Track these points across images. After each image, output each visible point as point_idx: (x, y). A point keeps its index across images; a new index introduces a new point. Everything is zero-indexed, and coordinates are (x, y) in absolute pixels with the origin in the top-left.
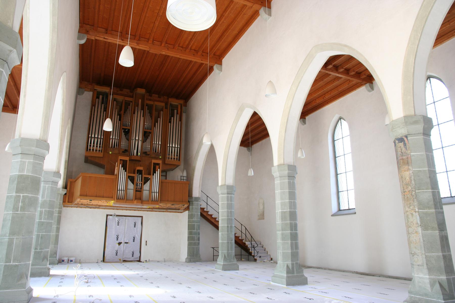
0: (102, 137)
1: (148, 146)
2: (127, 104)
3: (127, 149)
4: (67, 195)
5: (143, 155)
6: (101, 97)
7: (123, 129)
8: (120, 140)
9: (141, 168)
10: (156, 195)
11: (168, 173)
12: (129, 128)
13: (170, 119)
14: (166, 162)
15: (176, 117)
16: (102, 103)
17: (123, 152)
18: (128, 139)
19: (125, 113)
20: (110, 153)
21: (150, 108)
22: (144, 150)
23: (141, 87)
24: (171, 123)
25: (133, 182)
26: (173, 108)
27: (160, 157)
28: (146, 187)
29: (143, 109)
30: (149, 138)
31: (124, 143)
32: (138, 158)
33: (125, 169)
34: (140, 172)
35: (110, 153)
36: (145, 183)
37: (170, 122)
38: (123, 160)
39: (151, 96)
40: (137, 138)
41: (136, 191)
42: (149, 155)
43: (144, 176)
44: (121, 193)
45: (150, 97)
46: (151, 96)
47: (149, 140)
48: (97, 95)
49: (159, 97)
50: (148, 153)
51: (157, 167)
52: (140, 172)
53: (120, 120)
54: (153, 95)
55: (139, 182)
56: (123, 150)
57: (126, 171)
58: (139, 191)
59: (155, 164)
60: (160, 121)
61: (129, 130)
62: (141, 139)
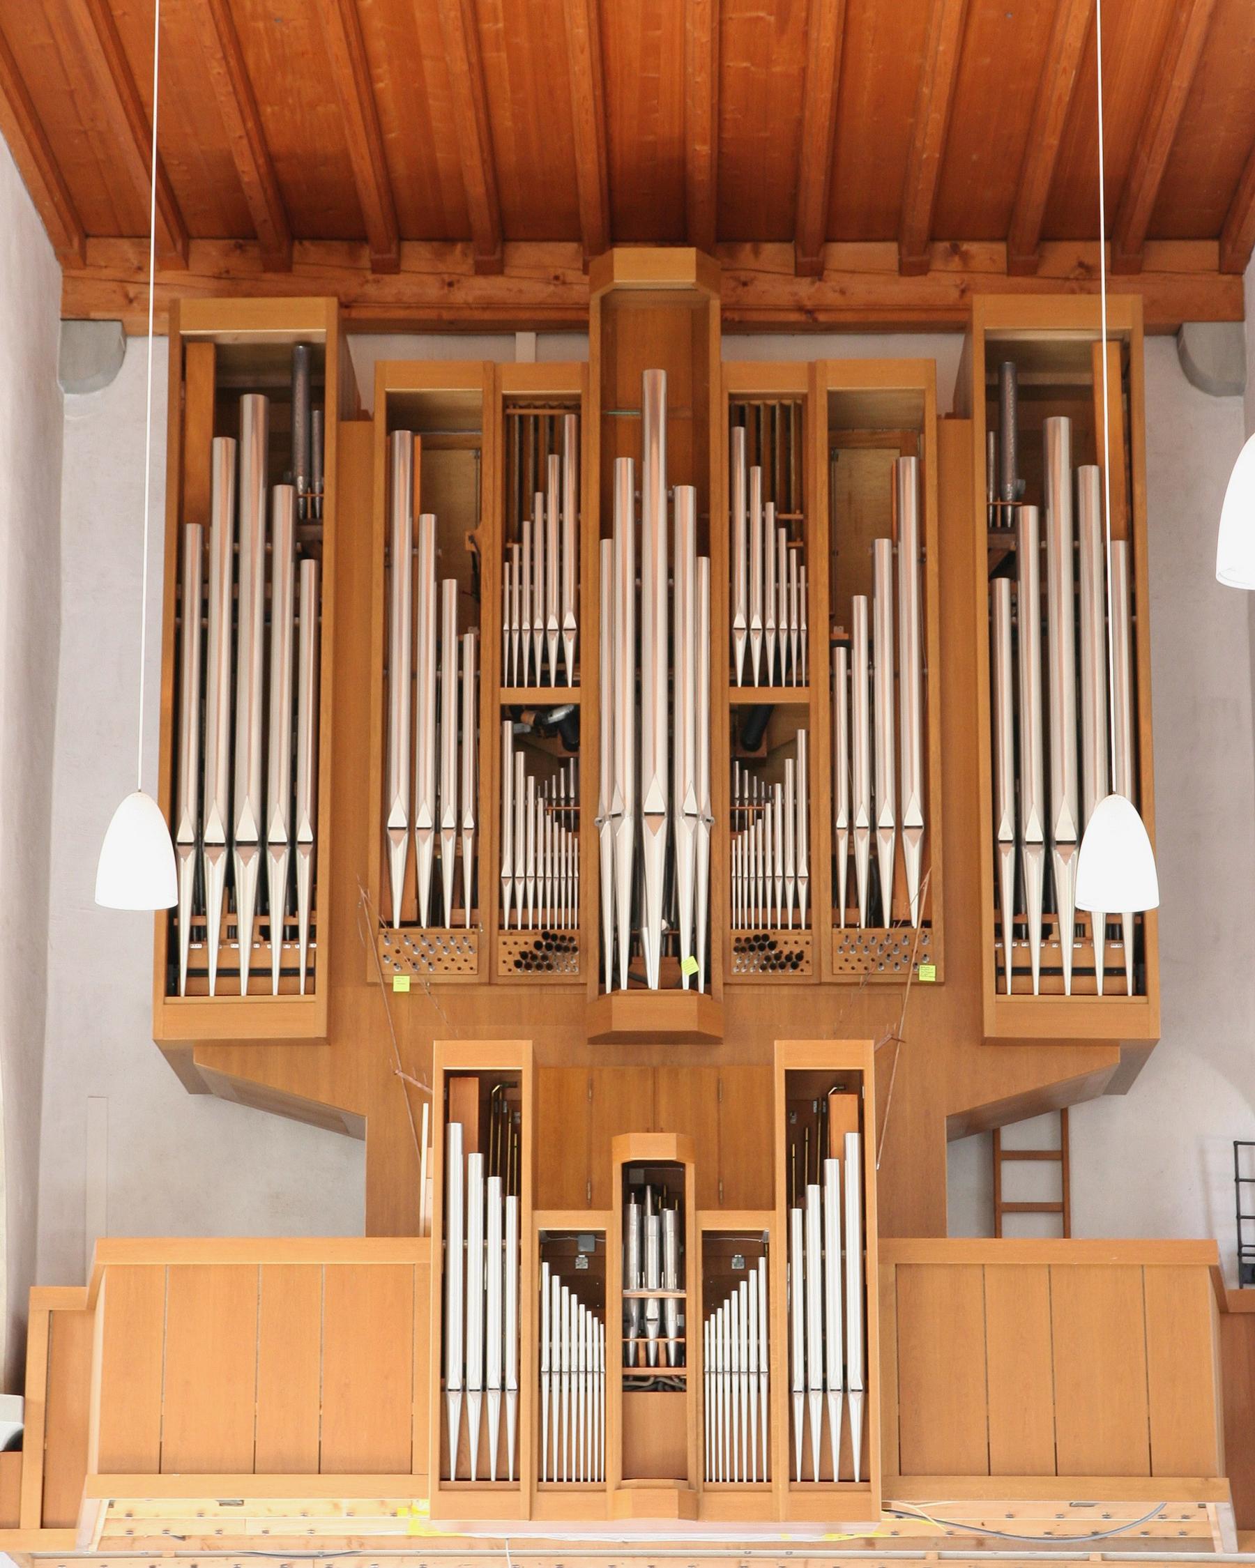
0: (305, 834)
1: (780, 853)
2: (530, 435)
3: (561, 917)
4: (32, 1444)
5: (745, 967)
6: (252, 408)
7: (512, 712)
8: (489, 830)
9: (658, 1147)
10: (837, 1417)
11: (1078, 1117)
12: (568, 695)
13: (1002, 525)
14: (989, 1032)
15: (1076, 492)
16: (277, 472)
17: (525, 961)
18: (570, 821)
19: (512, 534)
20: (401, 984)
21: (772, 429)
22: (749, 918)
23: (671, 234)
24: (1014, 577)
25: (590, 1293)
26: (1030, 395)
27: (928, 973)
28: (732, 1337)
29: (689, 466)
30: (794, 769)
31: (529, 855)
32: (679, 1013)
33: (500, 1160)
34: (654, 1185)
35: (401, 984)
36: (715, 1295)
37: (1005, 565)
38: (487, 1079)
39: (816, 272)
40: (655, 800)
41: (632, 1385)
42: (795, 961)
43: (702, 1221)
44: (481, 1420)
45: (804, 289)
46: (816, 272)
47: (789, 795)
48: (224, 385)
49: (908, 268)
50: (789, 942)
51: (841, 1107)
52: (654, 1185)
53: (469, 618)
54: (843, 253)
55: (657, 1289)
56: (526, 941)
57: (511, 1187)
58: (650, 1375)
59: (810, 1100)
60: (896, 563)
61: (574, 716)
62: (693, 799)
